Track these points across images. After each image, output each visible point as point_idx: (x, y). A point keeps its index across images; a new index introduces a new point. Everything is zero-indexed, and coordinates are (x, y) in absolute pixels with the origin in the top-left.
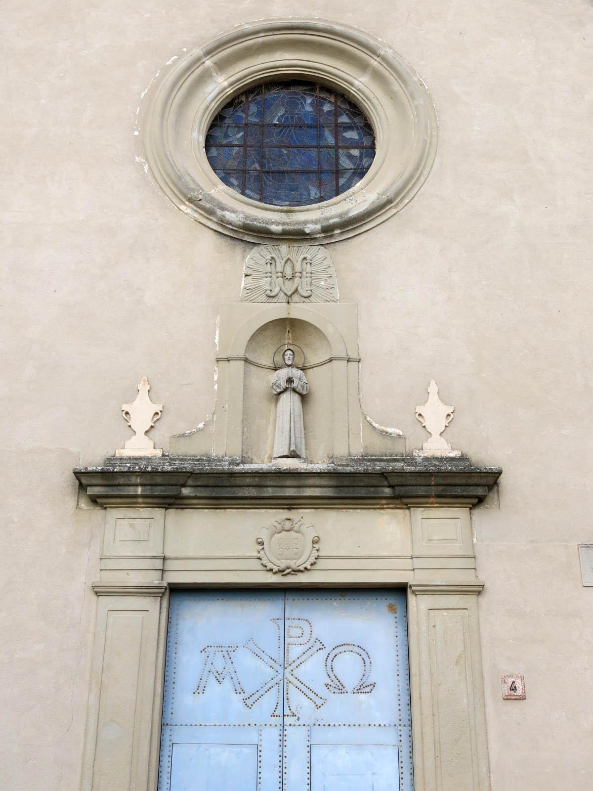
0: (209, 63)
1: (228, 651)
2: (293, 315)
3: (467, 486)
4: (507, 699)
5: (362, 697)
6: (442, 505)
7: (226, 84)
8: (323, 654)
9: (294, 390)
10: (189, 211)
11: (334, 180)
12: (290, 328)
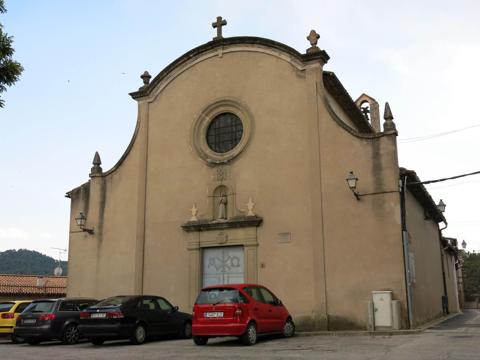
0: (203, 115)
1: (213, 259)
2: (223, 184)
3: (256, 222)
4: (261, 267)
5: (238, 267)
6: (250, 227)
7: (208, 119)
8: (231, 259)
9: (222, 203)
10: (200, 159)
11: (235, 141)
12: (222, 187)
